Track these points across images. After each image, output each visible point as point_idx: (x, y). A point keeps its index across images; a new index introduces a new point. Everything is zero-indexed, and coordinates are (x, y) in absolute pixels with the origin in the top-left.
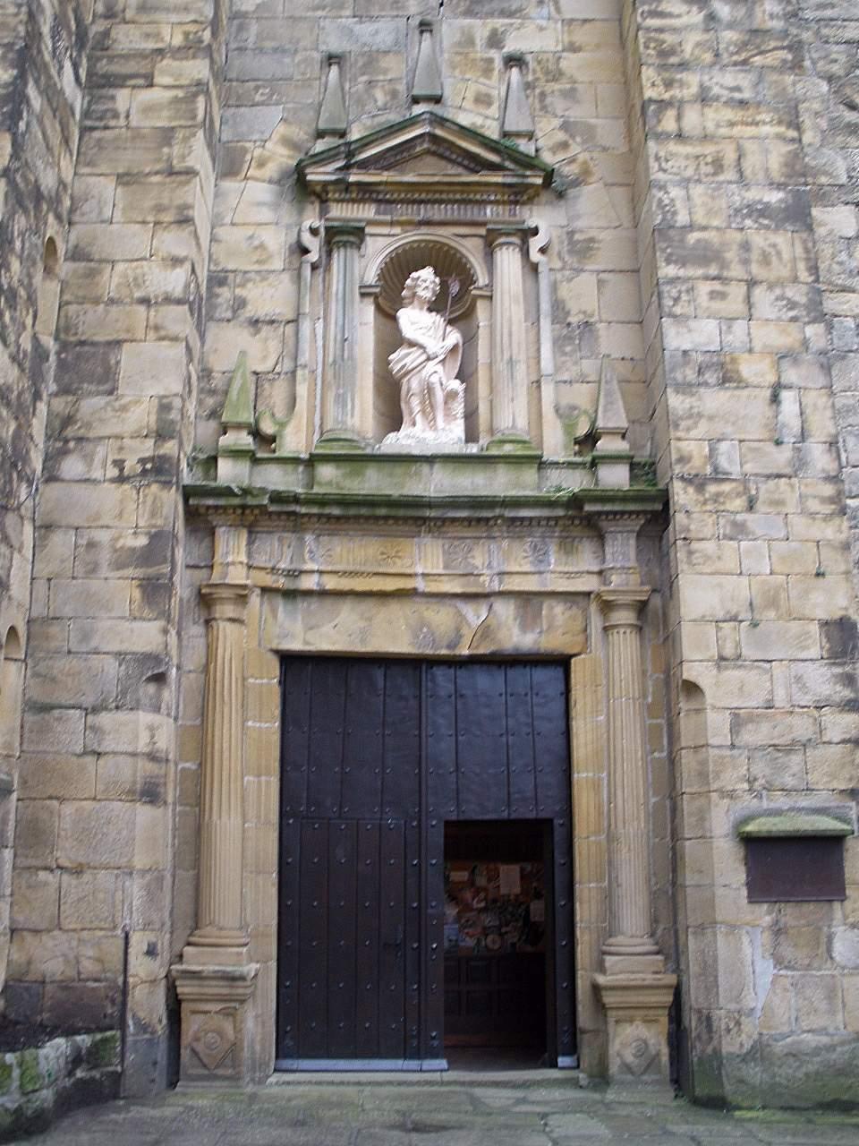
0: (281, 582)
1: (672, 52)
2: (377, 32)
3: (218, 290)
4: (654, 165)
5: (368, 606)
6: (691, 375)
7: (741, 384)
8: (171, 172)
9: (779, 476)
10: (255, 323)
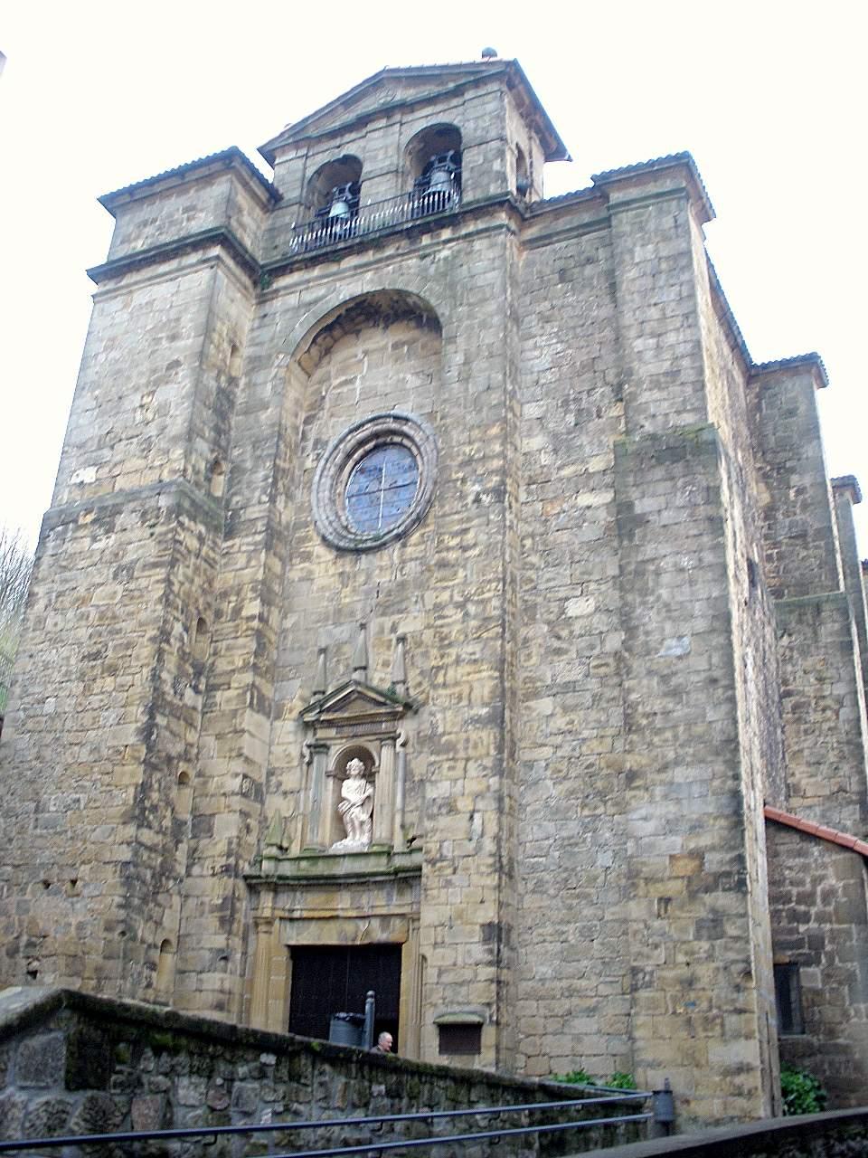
0: (287, 915)
1: (445, 638)
5: (321, 923)
7: (458, 812)
8: (236, 732)
10: (285, 793)
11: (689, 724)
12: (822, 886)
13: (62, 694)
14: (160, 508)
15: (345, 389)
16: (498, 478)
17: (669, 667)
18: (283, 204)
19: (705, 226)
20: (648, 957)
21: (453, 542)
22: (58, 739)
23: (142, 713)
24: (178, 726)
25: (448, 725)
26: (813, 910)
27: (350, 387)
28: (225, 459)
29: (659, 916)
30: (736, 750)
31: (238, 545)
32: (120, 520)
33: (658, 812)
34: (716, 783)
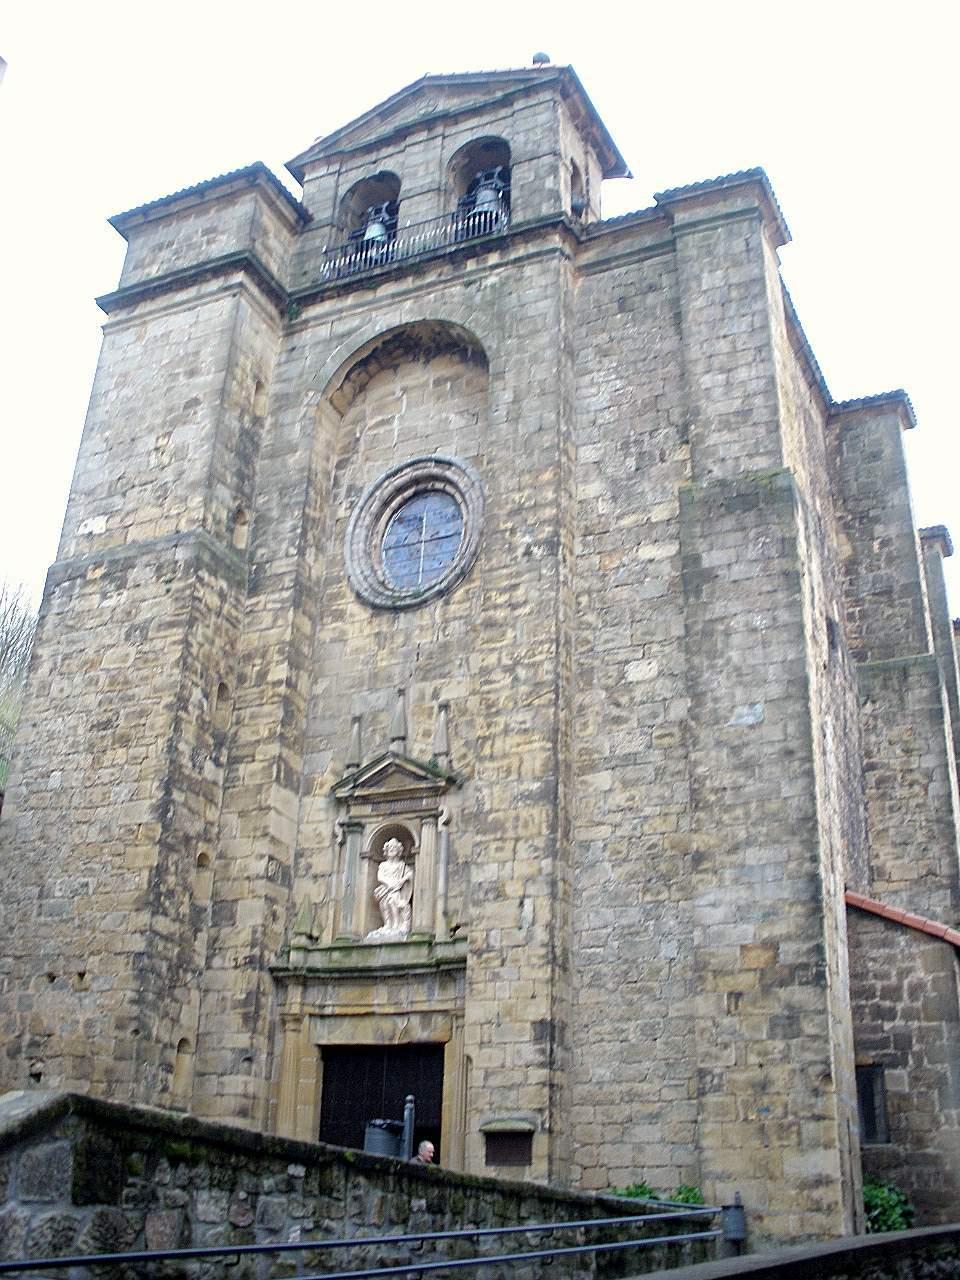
0: (317, 1011)
1: (492, 706)
5: (355, 1021)
7: (506, 898)
8: (261, 809)
10: (315, 877)
13: (68, 767)
14: (177, 562)
15: (381, 430)
17: (740, 737)
18: (313, 225)
20: (717, 1058)
21: (501, 600)
22: (64, 817)
23: (157, 788)
24: (197, 803)
25: (496, 802)
26: (900, 1006)
27: (388, 427)
28: (249, 507)
31: (263, 602)
32: (133, 575)
33: (728, 898)
34: (792, 865)
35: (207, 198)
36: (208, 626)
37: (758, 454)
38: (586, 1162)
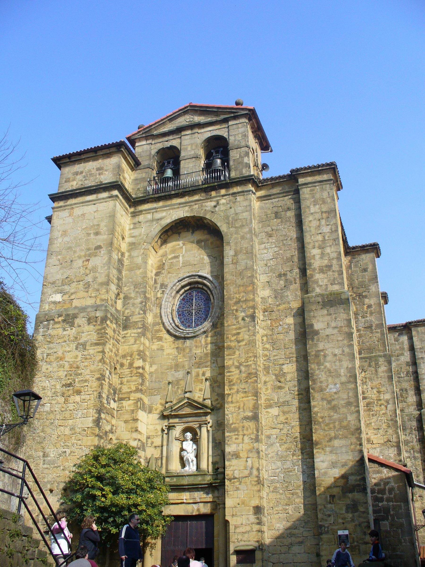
2: (179, 374)
3: (148, 440)
4: (226, 410)
6: (230, 457)
9: (246, 477)
10: (155, 447)
11: (341, 421)
12: (388, 486)
13: (53, 402)
14: (97, 317)
15: (174, 261)
16: (252, 310)
17: (331, 397)
18: (140, 167)
19: (338, 192)
20: (326, 520)
21: (233, 338)
22: (52, 423)
23: (95, 413)
24: (109, 418)
25: (235, 420)
26: (385, 497)
27: (177, 260)
28: (121, 292)
29: (330, 503)
30: (360, 433)
31: (130, 333)
32: (77, 321)
33: (328, 459)
34: (352, 447)
35: (98, 154)
36: (110, 344)
37: (335, 284)
38: (275, 561)
